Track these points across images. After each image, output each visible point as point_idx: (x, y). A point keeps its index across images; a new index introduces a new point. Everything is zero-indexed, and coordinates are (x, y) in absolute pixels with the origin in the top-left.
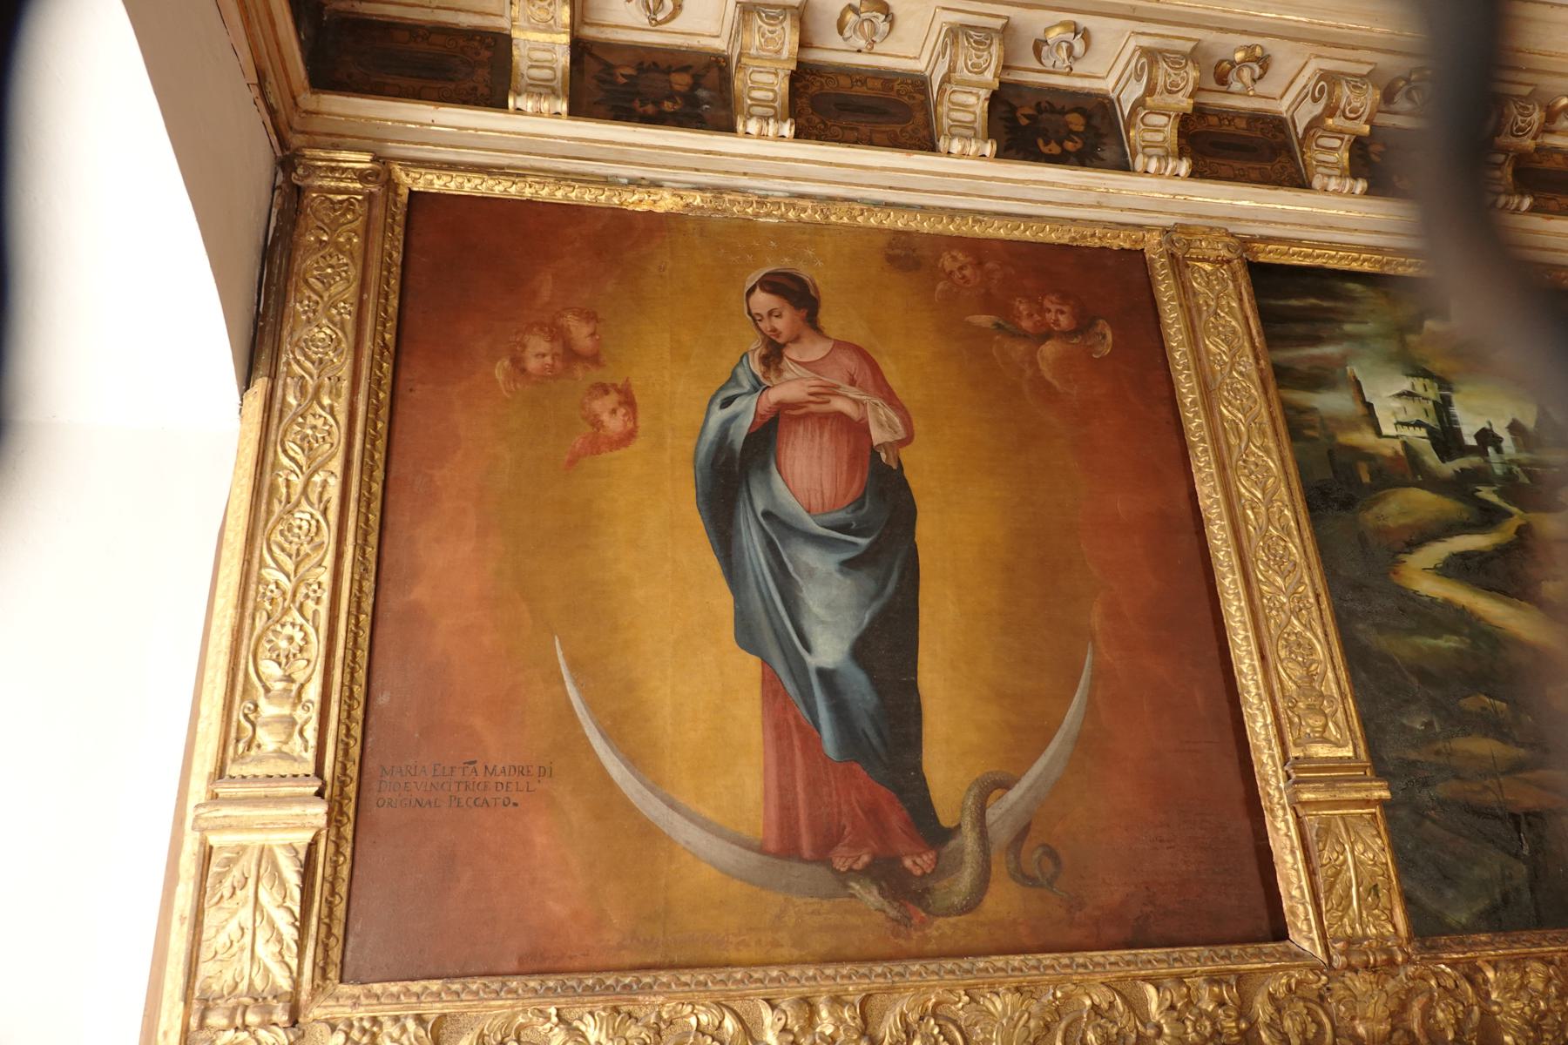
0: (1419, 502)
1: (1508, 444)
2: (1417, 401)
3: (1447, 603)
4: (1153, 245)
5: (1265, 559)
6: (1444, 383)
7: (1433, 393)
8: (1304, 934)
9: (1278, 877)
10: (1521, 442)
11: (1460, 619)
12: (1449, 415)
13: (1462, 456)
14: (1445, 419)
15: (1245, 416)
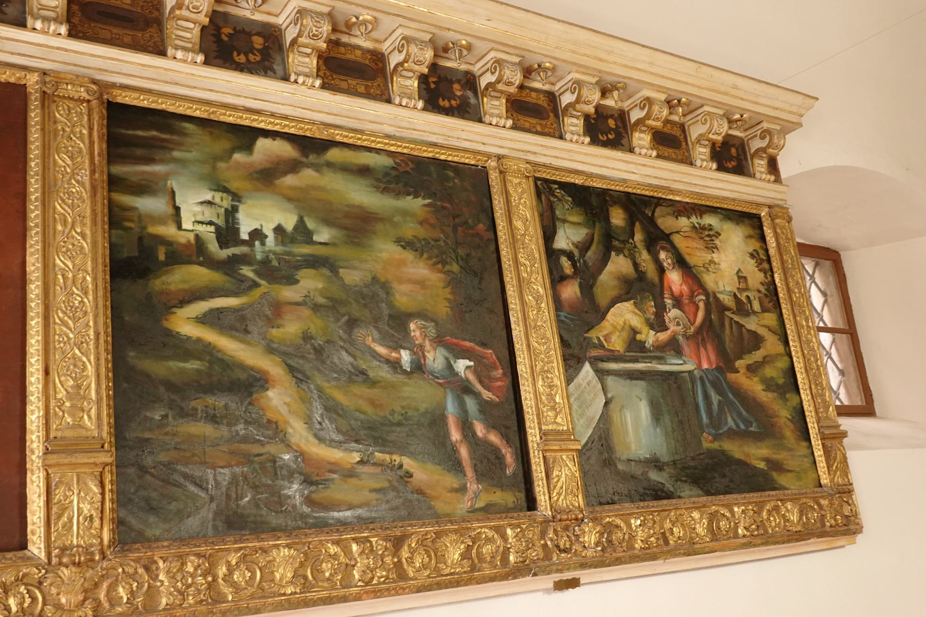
0: (199, 274)
1: (270, 240)
2: (213, 208)
3: (199, 340)
4: (32, 80)
5: (64, 309)
6: (237, 197)
7: (227, 203)
8: (36, 547)
9: (28, 511)
10: (280, 238)
11: (206, 351)
12: (234, 218)
13: (235, 246)
14: (231, 221)
15: (73, 211)
